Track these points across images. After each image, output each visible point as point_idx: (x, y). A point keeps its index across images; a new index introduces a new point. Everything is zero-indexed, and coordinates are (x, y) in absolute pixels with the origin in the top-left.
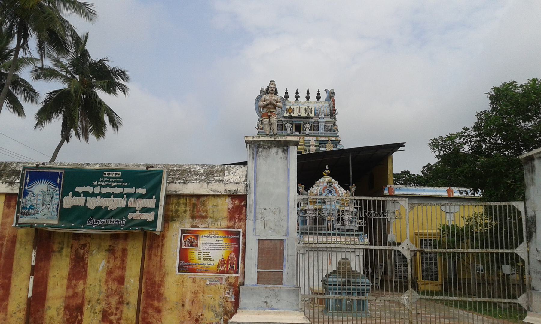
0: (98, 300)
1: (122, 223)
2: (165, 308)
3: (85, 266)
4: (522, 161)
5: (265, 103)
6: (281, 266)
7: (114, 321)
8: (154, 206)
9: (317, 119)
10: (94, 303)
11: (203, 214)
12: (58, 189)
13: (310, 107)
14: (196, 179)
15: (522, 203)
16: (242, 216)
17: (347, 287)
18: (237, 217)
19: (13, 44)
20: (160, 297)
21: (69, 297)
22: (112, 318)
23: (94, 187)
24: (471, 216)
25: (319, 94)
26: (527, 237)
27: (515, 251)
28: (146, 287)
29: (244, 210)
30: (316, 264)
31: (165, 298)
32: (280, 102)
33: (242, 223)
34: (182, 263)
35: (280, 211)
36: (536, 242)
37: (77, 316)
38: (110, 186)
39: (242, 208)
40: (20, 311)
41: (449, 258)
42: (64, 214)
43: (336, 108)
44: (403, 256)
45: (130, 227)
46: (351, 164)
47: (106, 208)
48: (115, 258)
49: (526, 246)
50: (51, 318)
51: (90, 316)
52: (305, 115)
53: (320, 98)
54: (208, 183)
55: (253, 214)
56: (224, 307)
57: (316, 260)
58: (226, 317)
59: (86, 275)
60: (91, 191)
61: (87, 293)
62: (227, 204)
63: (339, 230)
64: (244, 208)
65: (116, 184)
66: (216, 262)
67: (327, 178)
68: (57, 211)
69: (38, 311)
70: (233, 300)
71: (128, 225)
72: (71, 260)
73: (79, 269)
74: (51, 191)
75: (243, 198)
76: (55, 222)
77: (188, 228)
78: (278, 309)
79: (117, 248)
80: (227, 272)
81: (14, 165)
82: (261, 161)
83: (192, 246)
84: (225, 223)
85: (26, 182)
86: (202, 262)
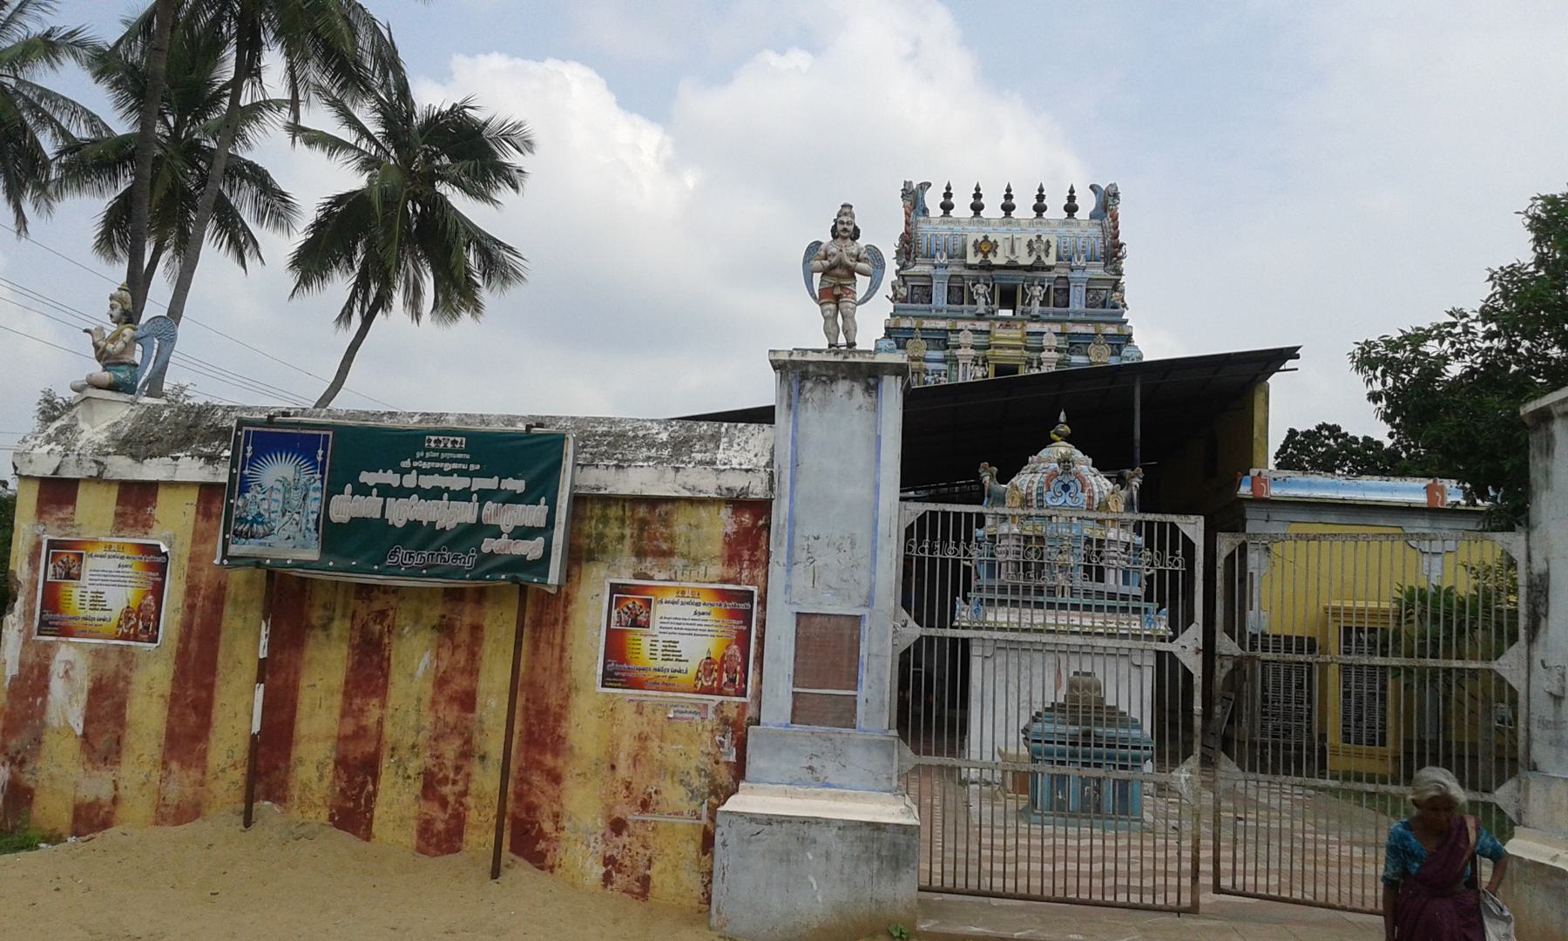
0: (414, 746)
1: (468, 563)
2: (570, 771)
3: (385, 664)
4: (1527, 421)
5: (826, 263)
6: (854, 682)
7: (451, 799)
8: (543, 524)
9: (1063, 272)
10: (404, 752)
11: (665, 547)
12: (318, 476)
13: (1044, 239)
14: (648, 458)
15: (1522, 538)
16: (758, 553)
17: (1093, 749)
18: (746, 554)
19: (227, 70)
20: (557, 744)
21: (346, 737)
22: (447, 790)
23: (403, 472)
24: (1489, 562)
25: (1071, 198)
26: (1526, 628)
27: (1494, 665)
28: (526, 719)
29: (763, 539)
30: (1012, 688)
31: (571, 748)
32: (865, 260)
33: (759, 572)
34: (48, 615)
35: (853, 544)
36: (1545, 644)
37: (365, 783)
38: (441, 472)
39: (759, 536)
40: (234, 766)
41: (1422, 683)
42: (333, 536)
43: (1121, 239)
44: (1185, 668)
45: (488, 572)
46: (1138, 408)
47: (432, 524)
48: (455, 648)
49: (1524, 652)
50: (306, 786)
51: (394, 784)
52: (1028, 261)
53: (1076, 209)
54: (677, 469)
55: (784, 549)
56: (711, 776)
57: (1000, 678)
58: (714, 800)
59: (385, 686)
60: (396, 484)
61: (388, 728)
62: (723, 522)
63: (1087, 594)
64: (765, 533)
65: (455, 466)
66: (692, 667)
67: (1062, 448)
68: (317, 530)
69: (277, 768)
70: (733, 759)
71: (480, 570)
72: (352, 647)
73: (369, 672)
74: (303, 480)
75: (762, 508)
76: (313, 554)
77: (627, 579)
78: (841, 787)
79: (458, 623)
80: (720, 692)
81: (220, 413)
82: (809, 414)
83: (635, 623)
84: (716, 570)
85: (244, 457)
86: (659, 663)
